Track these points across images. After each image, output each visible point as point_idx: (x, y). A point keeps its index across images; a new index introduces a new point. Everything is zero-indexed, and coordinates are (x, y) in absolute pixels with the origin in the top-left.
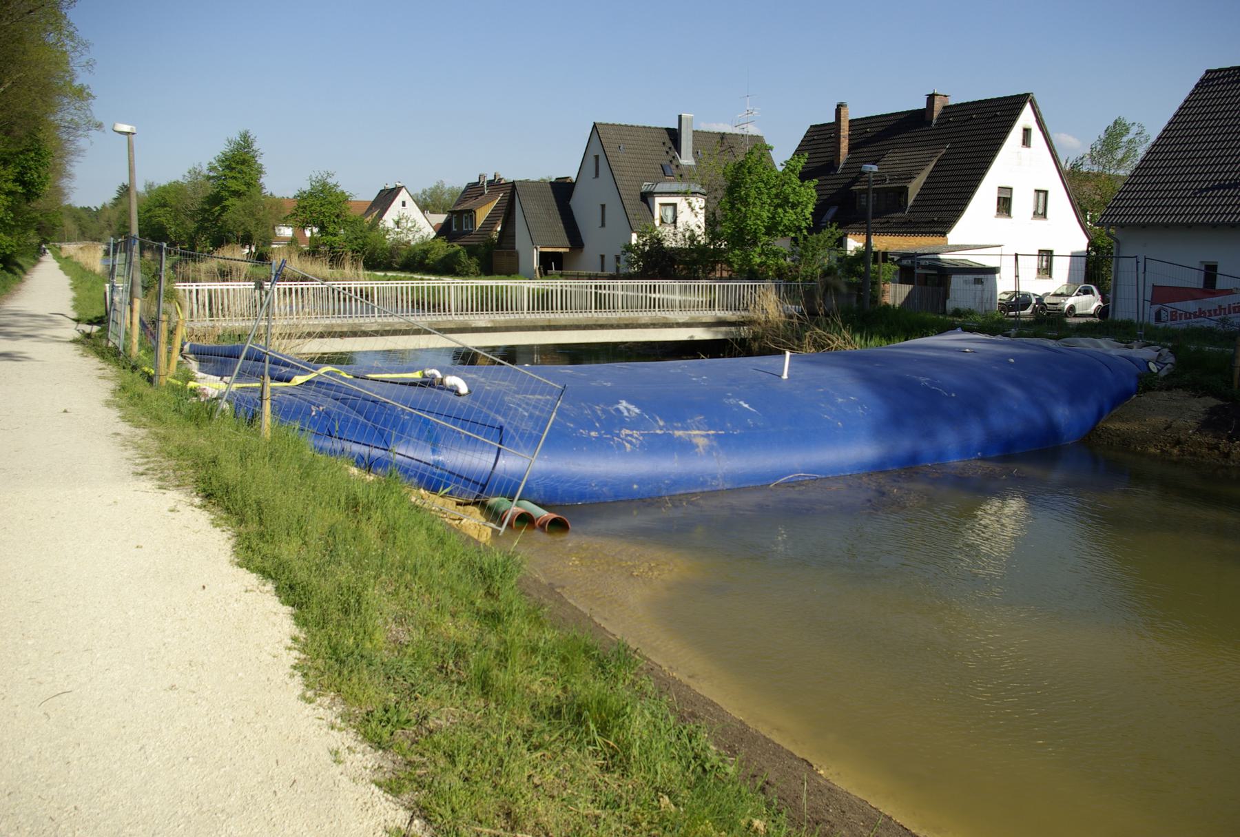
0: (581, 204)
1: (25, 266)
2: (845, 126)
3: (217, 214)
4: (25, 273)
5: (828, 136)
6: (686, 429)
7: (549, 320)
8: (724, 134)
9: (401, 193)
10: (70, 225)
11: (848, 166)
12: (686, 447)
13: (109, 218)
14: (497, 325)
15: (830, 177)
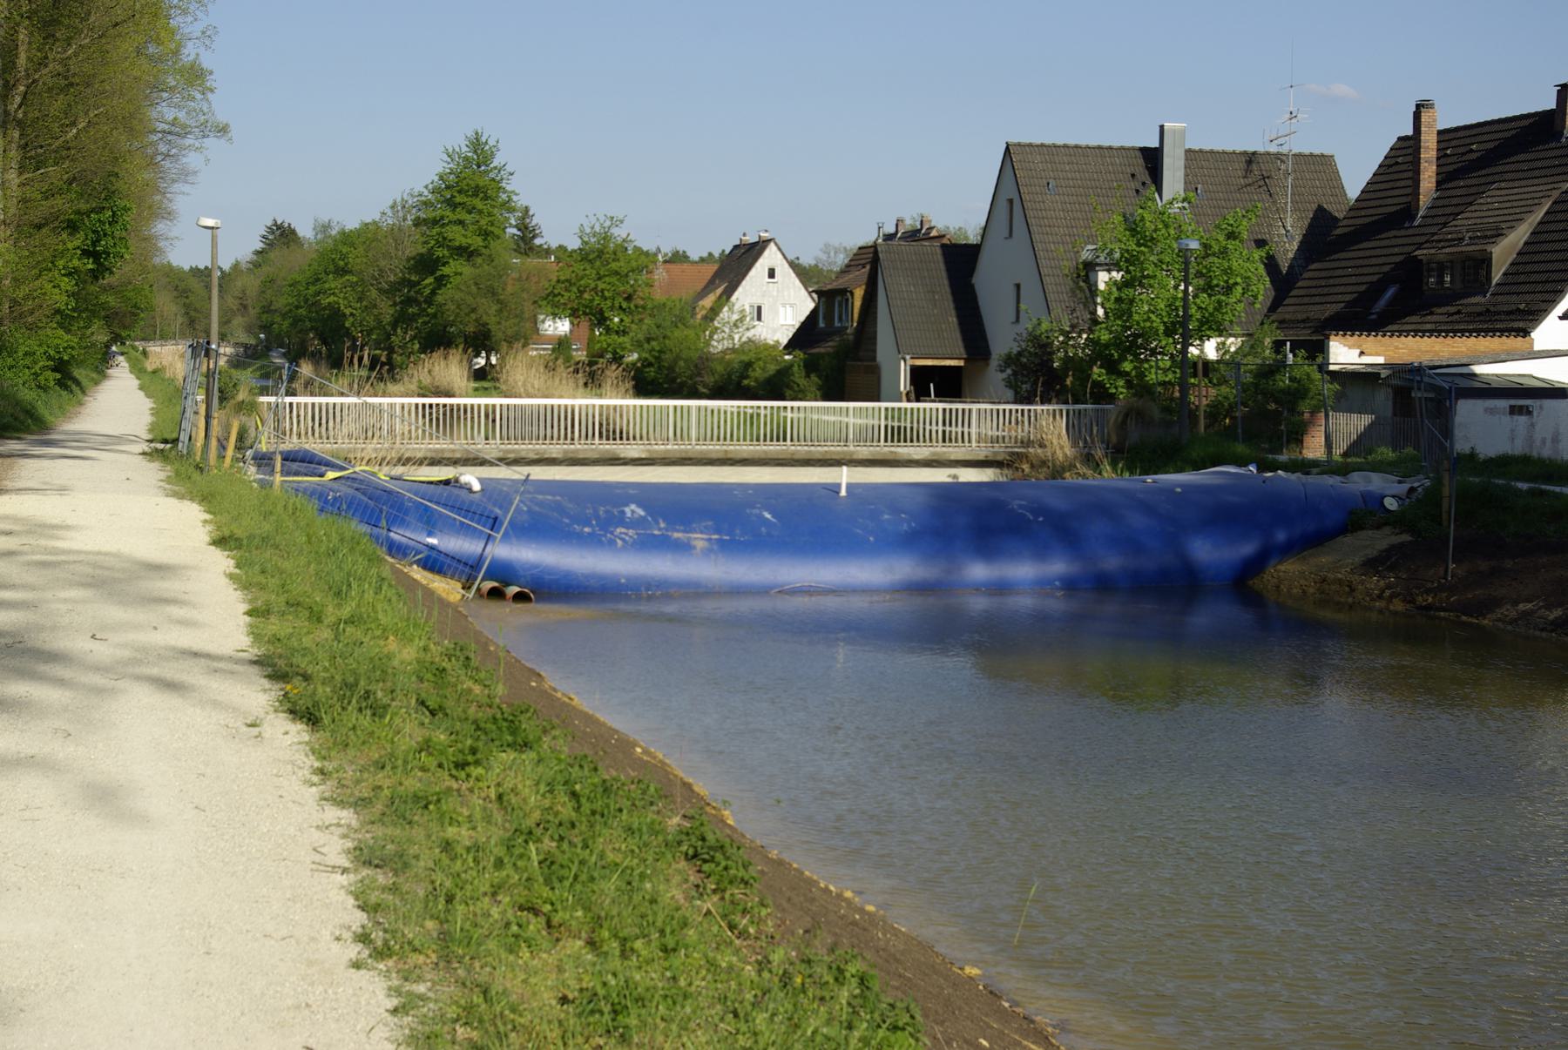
0: (990, 283)
1: (84, 382)
2: (1429, 142)
3: (427, 291)
4: (84, 392)
5: (1467, 148)
6: (687, 532)
7: (726, 451)
8: (1254, 153)
9: (766, 253)
10: (166, 305)
11: (1434, 212)
12: (684, 548)
13: (244, 292)
14: (655, 456)
15: (1403, 232)
